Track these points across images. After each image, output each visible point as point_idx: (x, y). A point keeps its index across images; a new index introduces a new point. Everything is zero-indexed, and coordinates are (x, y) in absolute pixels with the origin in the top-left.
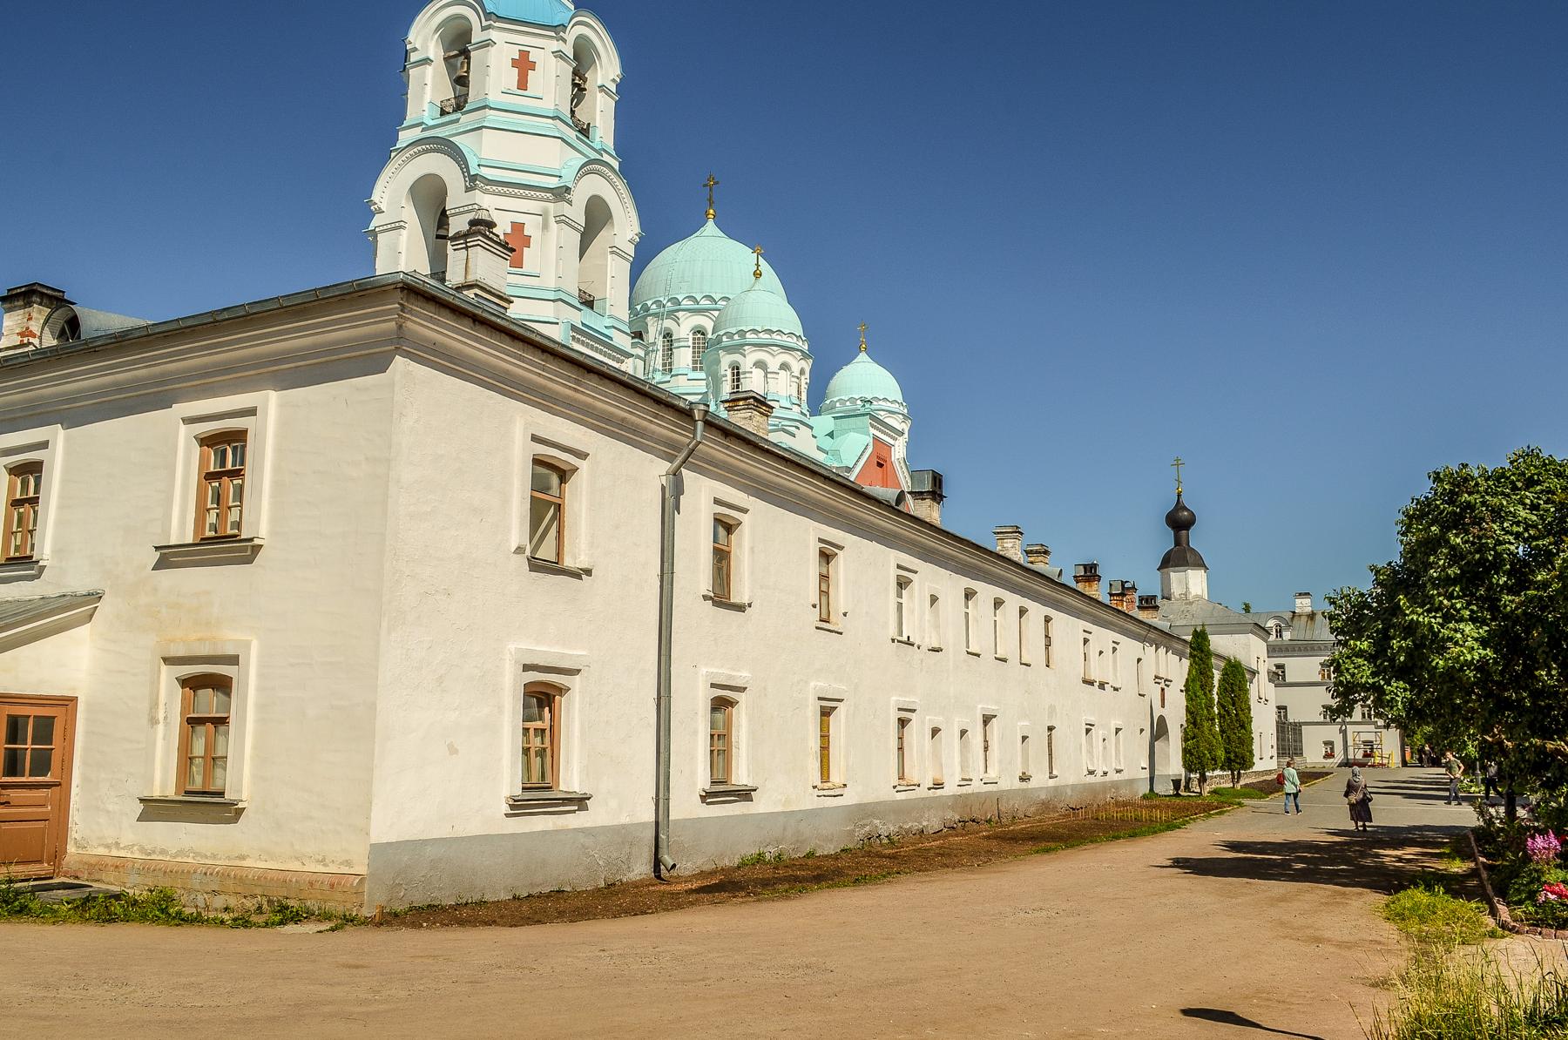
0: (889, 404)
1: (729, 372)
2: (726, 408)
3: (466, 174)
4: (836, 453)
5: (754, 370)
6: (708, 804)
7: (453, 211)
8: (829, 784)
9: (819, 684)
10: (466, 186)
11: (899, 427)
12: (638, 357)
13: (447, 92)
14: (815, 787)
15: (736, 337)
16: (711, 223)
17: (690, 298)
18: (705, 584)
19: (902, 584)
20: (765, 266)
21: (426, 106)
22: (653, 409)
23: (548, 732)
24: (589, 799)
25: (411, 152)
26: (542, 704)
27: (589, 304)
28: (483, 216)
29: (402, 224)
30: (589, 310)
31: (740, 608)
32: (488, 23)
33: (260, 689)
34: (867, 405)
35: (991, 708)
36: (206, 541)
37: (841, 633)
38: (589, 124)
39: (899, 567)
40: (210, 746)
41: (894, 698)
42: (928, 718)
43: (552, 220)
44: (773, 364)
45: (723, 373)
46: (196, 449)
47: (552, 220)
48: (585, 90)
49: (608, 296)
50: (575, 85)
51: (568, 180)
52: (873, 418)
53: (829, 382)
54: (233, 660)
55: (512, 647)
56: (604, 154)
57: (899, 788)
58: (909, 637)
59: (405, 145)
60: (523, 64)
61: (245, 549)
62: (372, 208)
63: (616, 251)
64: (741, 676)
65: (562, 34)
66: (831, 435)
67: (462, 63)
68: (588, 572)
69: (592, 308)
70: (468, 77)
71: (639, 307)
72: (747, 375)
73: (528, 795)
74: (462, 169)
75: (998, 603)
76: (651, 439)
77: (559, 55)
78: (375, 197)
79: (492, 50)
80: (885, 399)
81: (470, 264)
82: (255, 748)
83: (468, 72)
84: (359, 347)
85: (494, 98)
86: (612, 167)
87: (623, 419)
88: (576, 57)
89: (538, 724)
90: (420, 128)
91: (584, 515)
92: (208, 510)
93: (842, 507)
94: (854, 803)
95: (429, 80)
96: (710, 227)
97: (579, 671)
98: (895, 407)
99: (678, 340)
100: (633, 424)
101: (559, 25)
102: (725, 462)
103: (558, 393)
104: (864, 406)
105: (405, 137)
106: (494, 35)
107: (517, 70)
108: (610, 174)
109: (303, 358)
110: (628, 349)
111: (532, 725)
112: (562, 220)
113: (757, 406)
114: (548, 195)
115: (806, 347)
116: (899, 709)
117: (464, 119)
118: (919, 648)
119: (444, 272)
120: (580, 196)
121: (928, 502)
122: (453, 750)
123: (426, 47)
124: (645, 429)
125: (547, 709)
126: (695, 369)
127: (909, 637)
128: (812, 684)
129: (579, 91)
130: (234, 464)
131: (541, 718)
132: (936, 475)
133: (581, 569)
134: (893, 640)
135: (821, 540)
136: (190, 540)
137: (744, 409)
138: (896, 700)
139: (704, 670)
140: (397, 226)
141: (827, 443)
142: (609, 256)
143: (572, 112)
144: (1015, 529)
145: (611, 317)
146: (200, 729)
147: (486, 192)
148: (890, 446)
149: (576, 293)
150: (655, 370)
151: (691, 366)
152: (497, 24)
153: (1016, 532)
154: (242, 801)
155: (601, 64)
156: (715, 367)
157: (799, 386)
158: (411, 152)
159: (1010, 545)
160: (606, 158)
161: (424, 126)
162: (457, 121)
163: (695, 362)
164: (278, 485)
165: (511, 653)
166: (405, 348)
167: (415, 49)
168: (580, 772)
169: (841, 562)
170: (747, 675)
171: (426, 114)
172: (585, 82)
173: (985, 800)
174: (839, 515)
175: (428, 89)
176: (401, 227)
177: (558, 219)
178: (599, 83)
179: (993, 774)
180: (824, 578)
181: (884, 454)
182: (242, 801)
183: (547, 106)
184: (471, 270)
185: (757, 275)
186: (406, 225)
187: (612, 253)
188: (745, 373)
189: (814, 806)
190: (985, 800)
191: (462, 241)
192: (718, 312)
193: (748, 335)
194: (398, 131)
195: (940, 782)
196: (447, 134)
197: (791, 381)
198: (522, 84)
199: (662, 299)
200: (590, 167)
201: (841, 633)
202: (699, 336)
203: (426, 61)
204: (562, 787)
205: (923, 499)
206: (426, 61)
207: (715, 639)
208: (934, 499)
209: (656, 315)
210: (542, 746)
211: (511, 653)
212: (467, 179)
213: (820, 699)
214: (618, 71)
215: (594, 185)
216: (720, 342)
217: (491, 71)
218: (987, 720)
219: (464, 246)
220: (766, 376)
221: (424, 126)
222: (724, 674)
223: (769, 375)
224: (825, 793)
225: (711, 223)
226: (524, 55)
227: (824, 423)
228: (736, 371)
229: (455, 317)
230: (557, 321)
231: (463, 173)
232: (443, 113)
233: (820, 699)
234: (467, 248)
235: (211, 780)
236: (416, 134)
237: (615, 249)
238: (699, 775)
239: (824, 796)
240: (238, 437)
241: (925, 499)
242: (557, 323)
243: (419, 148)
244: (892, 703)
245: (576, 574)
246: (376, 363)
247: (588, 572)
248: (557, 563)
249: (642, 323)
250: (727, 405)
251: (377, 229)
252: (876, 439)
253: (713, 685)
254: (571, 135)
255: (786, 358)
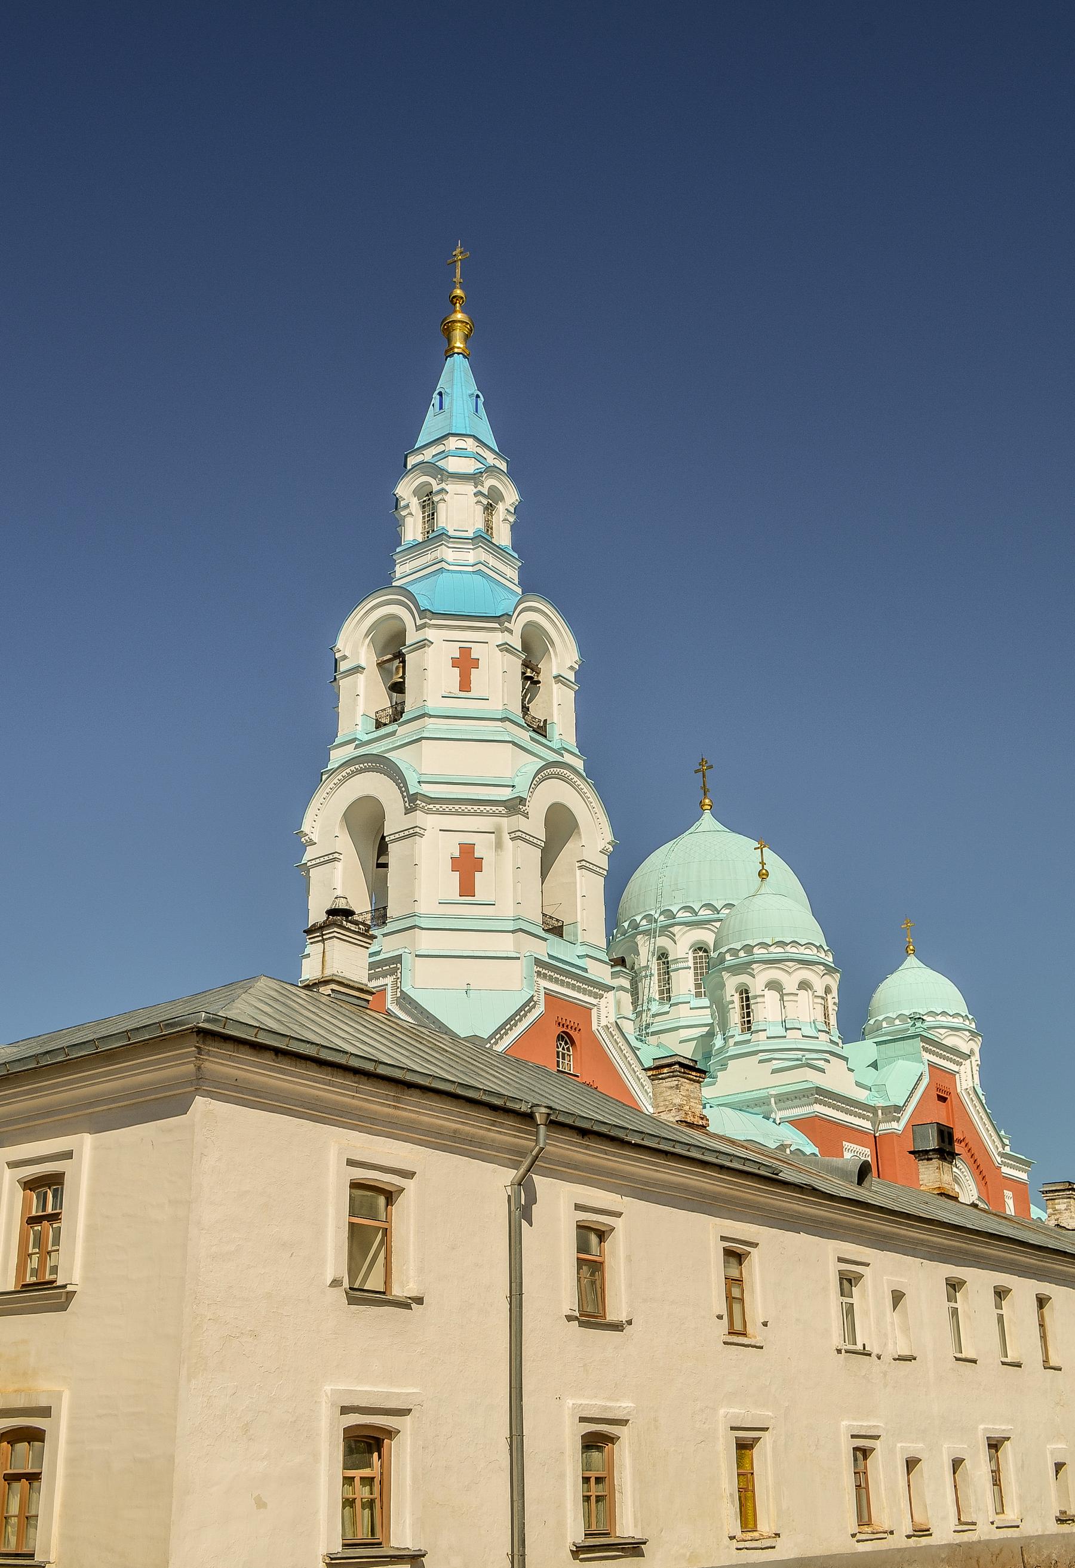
0: (950, 1019)
1: (737, 998)
2: (649, 1077)
3: (405, 794)
4: (881, 1088)
5: (767, 992)
6: (582, 1560)
7: (392, 837)
8: (755, 1535)
9: (732, 1410)
10: (406, 808)
11: (965, 1048)
12: (622, 988)
13: (383, 701)
14: (732, 1538)
15: (742, 954)
16: (707, 815)
17: (688, 909)
18: (569, 1302)
19: (848, 1281)
20: (774, 861)
21: (359, 720)
22: (489, 1116)
23: (377, 1481)
24: (424, 1556)
25: (344, 774)
26: (371, 1449)
27: (557, 931)
28: (342, 904)
29: (336, 855)
30: (557, 939)
31: (617, 1327)
32: (423, 621)
33: (71, 1442)
34: (918, 1024)
35: (999, 1429)
36: (27, 1287)
37: (762, 1348)
38: (545, 721)
39: (841, 1260)
40: (25, 1504)
41: (844, 1423)
42: (899, 1445)
43: (506, 837)
44: (790, 983)
45: (729, 999)
46: (20, 1193)
47: (506, 837)
48: (539, 682)
49: (579, 920)
50: (526, 678)
51: (522, 790)
52: (925, 1039)
53: (871, 997)
54: (45, 1412)
55: (328, 1388)
56: (566, 754)
57: (859, 1537)
58: (864, 1345)
59: (337, 766)
60: (465, 663)
61: (59, 1296)
62: (303, 840)
63: (585, 865)
64: (622, 1406)
65: (506, 624)
66: (874, 1065)
67: (397, 668)
68: (419, 1301)
69: (561, 936)
70: (404, 682)
71: (626, 925)
72: (759, 1000)
73: (592, 1541)
74: (400, 788)
75: (1001, 1293)
76: (491, 1147)
77: (505, 648)
78: (306, 828)
79: (429, 650)
80: (944, 1013)
81: (326, 958)
82: (65, 1505)
83: (403, 677)
84: (155, 1090)
85: (434, 704)
86: (576, 770)
87: (455, 1131)
88: (526, 647)
89: (366, 1472)
90: (354, 745)
91: (412, 1239)
92: (30, 1255)
93: (751, 1197)
94: (792, 1557)
95: (361, 690)
96: (707, 820)
97: (410, 1410)
98: (957, 1022)
99: (676, 961)
100: (467, 1134)
101: (503, 615)
102: (587, 1163)
103: (376, 1113)
104: (914, 1025)
105: (338, 756)
106: (430, 634)
107: (457, 670)
108: (572, 776)
109: (114, 1100)
110: (608, 981)
111: (357, 1473)
112: (517, 836)
113: (684, 1073)
114: (500, 809)
115: (829, 959)
116: (853, 1436)
117: (402, 730)
118: (879, 1358)
119: (385, 908)
120: (538, 807)
121: (936, 1162)
122: (260, 1504)
123: (356, 653)
124: (483, 1138)
125: (376, 1455)
126: (698, 995)
127: (864, 1345)
128: (722, 1411)
129: (531, 681)
130: (54, 1208)
131: (369, 1465)
132: (943, 1128)
133: (409, 1298)
134: (839, 1351)
135: (723, 1238)
136: (11, 1287)
137: (669, 1077)
138: (847, 1425)
139: (570, 1402)
140: (331, 859)
141: (870, 1077)
142: (578, 872)
143: (525, 709)
144: (1067, 1186)
145: (583, 944)
146: (16, 1486)
147: (429, 812)
148: (953, 1074)
149: (539, 919)
150: (649, 1001)
151: (693, 991)
152: (433, 622)
153: (1069, 1190)
154: (49, 1563)
155: (555, 651)
156: (720, 992)
157: (826, 1008)
158: (344, 774)
159: (1063, 1207)
160: (568, 758)
161: (357, 742)
162: (394, 733)
163: (698, 986)
164: (91, 1229)
165: (327, 1396)
166: (204, 1088)
167: (345, 657)
168: (413, 1525)
169: (755, 1268)
170: (630, 1405)
171: (359, 728)
172: (538, 674)
173: (1001, 1550)
174: (750, 1207)
175: (361, 700)
176: (334, 860)
177: (513, 835)
178: (555, 673)
179: (1011, 1514)
180: (734, 1282)
181: (946, 1084)
182: (49, 1563)
183: (495, 707)
184: (327, 965)
185: (763, 875)
186: (341, 857)
187: (581, 868)
188: (756, 997)
189: (734, 1562)
190: (1001, 1550)
191: (318, 934)
192: (718, 924)
193: (756, 950)
194: (330, 749)
195: (924, 1527)
196: (383, 749)
197: (814, 1003)
198: (465, 685)
199: (652, 912)
200: (548, 771)
201: (762, 1348)
202: (701, 954)
203: (358, 669)
204: (394, 1543)
205: (929, 1159)
206: (358, 669)
207: (585, 1365)
208: (943, 1158)
209: (644, 932)
210: (371, 1496)
211: (327, 1396)
212: (406, 799)
213: (732, 1428)
214: (576, 657)
215: (555, 791)
216: (723, 961)
217: (429, 674)
218: (994, 1445)
219: (320, 938)
220: (782, 999)
221: (357, 742)
222: (596, 1404)
223: (785, 998)
224: (748, 1544)
225: (707, 815)
226: (465, 652)
227: (863, 1051)
228: (744, 995)
229: (256, 1052)
230: (518, 955)
231: (402, 792)
232: (379, 725)
233: (732, 1428)
234: (323, 941)
235: (24, 1539)
236: (349, 752)
237: (584, 863)
238: (569, 1526)
239: (746, 1548)
240: (54, 1181)
241: (931, 1159)
242: (518, 958)
243: (352, 768)
244: (843, 1430)
245: (404, 1304)
246: (181, 1107)
247: (419, 1301)
248: (384, 1293)
249: (630, 944)
250: (650, 1073)
251: (309, 864)
252: (932, 1066)
253: (582, 1420)
254: (525, 736)
255: (805, 974)
